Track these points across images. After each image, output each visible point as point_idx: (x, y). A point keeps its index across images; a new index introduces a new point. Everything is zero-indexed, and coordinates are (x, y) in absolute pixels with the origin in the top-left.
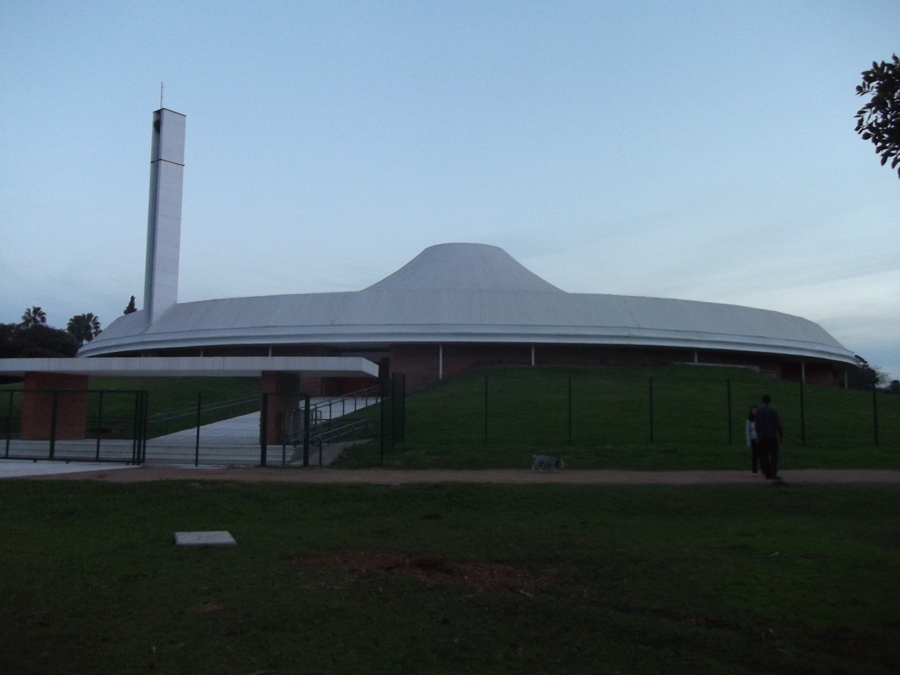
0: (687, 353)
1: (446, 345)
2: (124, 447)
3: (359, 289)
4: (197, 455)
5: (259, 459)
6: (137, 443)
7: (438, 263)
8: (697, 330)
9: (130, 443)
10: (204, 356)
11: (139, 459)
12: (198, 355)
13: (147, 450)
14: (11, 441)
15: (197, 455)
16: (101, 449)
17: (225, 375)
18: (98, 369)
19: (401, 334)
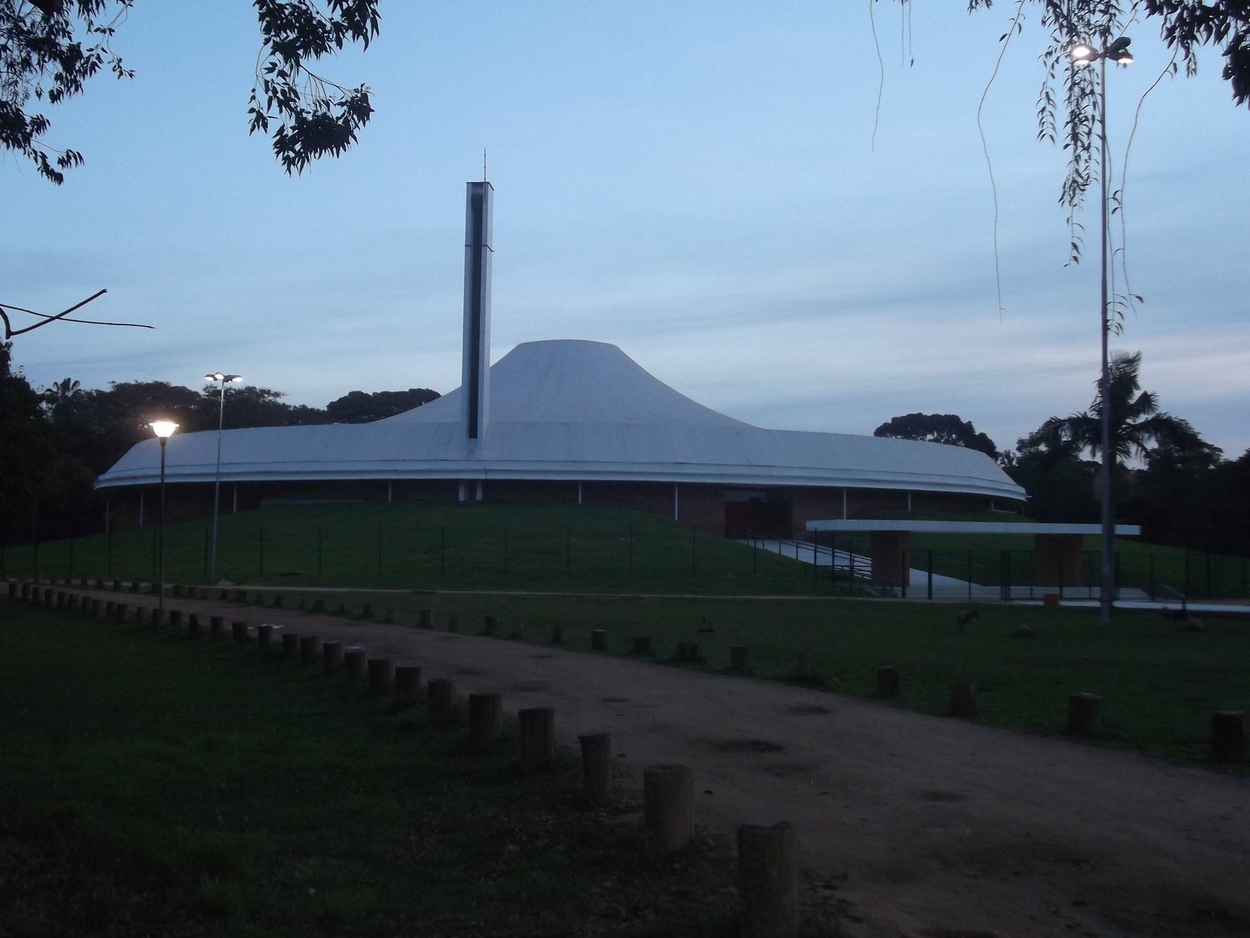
1: (586, 484)
11: (1006, 597)
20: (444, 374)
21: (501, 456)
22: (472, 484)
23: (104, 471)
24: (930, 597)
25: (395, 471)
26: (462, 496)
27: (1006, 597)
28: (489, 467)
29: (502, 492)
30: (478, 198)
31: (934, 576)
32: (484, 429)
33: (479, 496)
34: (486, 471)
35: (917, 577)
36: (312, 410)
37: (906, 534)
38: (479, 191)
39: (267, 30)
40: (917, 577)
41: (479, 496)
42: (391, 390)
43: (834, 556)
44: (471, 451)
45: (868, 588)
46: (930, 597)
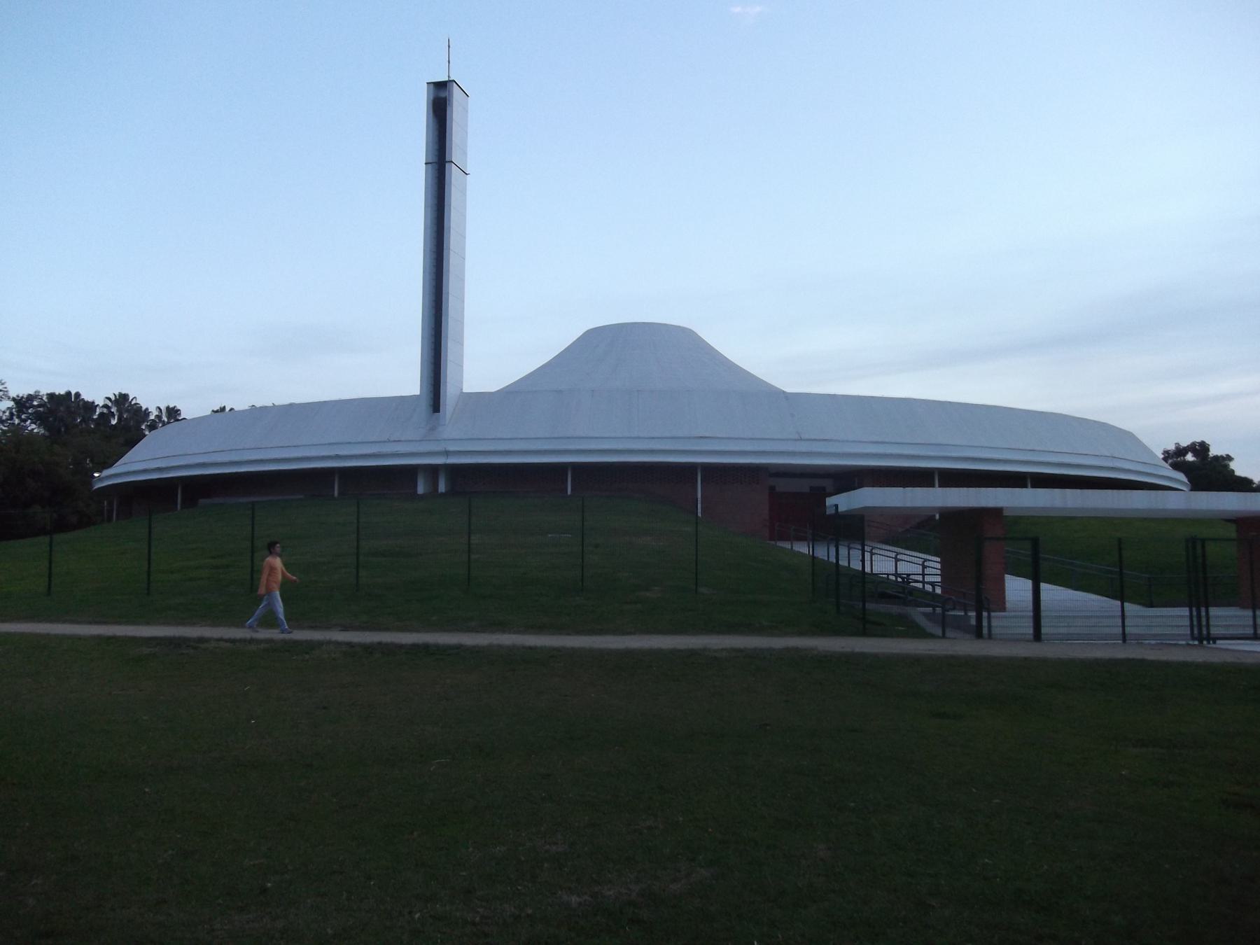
0: (680, 475)
1: (577, 467)
2: (1176, 618)
3: (788, 390)
4: (1123, 626)
5: (1031, 631)
6: (1195, 613)
7: (608, 348)
8: (933, 441)
9: (1185, 611)
10: (1033, 487)
11: (1202, 635)
12: (1025, 486)
13: (1187, 623)
14: (993, 614)
15: (1123, 626)
16: (1127, 623)
17: (1045, 514)
18: (1048, 505)
19: (652, 452)
20: (407, 380)
21: (460, 442)
22: (433, 470)
24: (1037, 636)
25: (338, 457)
26: (421, 489)
27: (1202, 635)
28: (451, 448)
29: (478, 482)
30: (441, 101)
31: (1126, 604)
32: (448, 415)
33: (442, 487)
34: (447, 453)
35: (1017, 589)
36: (256, 413)
37: (996, 513)
38: (442, 95)
39: (168, 408)
40: (1017, 589)
41: (442, 487)
42: (240, 403)
43: (897, 560)
44: (433, 429)
45: (918, 614)
46: (1037, 636)
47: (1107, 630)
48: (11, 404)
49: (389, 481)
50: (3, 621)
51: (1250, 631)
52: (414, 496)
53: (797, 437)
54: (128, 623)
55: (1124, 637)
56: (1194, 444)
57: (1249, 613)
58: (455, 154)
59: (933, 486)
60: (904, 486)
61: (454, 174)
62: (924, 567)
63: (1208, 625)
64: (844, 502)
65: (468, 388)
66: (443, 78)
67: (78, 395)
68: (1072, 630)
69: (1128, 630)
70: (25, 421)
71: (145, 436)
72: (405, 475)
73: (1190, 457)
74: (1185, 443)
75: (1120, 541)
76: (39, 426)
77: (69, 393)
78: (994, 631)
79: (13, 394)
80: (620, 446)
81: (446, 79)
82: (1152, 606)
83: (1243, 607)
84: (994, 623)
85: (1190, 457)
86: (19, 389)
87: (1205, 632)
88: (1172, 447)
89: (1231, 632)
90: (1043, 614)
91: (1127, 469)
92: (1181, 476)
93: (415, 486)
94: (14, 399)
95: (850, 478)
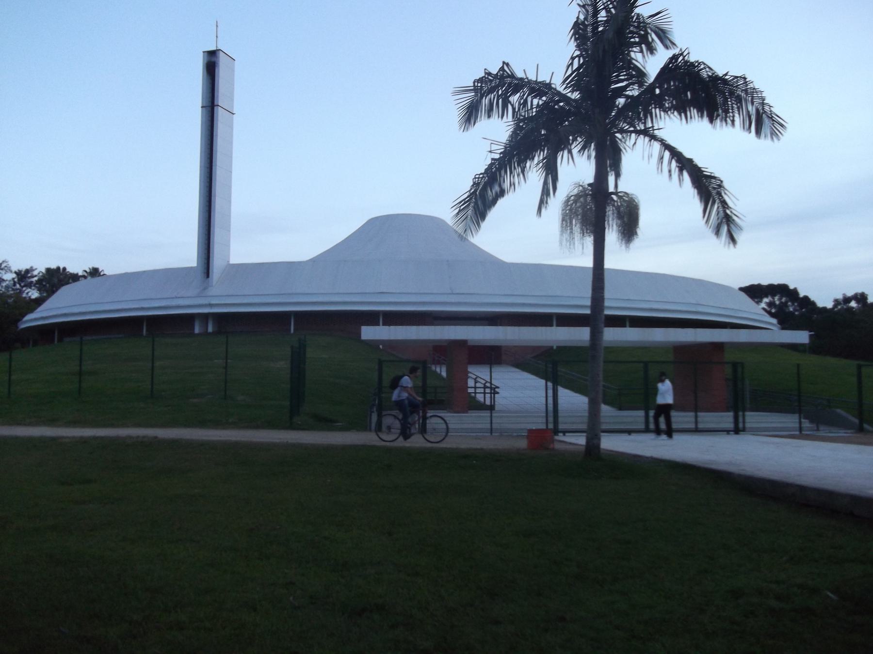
12: (624, 326)
16: (489, 419)
20: (187, 255)
21: (223, 297)
22: (205, 317)
23: (596, 157)
25: (142, 309)
29: (230, 323)
33: (210, 329)
34: (211, 305)
38: (213, 59)
41: (210, 329)
44: (205, 289)
47: (480, 426)
48: (14, 276)
49: (180, 323)
50: (4, 424)
51: (693, 426)
52: (192, 334)
53: (450, 291)
54: (112, 426)
55: (491, 431)
56: (856, 295)
57: (692, 414)
58: (221, 99)
59: (551, 325)
60: (419, 325)
61: (220, 113)
62: (476, 383)
63: (744, 422)
64: (369, 333)
65: (234, 260)
66: (213, 48)
67: (64, 269)
68: (465, 426)
69: (494, 426)
70: (23, 287)
71: (758, 303)
72: (189, 319)
73: (853, 304)
74: (850, 294)
75: (798, 365)
76: (767, 296)
77: (58, 268)
78: (748, 425)
79: (15, 268)
80: (245, 301)
81: (214, 49)
82: (620, 409)
83: (691, 411)
84: (748, 419)
85: (853, 304)
86: (19, 264)
87: (741, 425)
88: (840, 297)
89: (574, 427)
90: (560, 415)
91: (710, 310)
92: (774, 321)
93: (194, 329)
94: (16, 273)
95: (372, 318)
